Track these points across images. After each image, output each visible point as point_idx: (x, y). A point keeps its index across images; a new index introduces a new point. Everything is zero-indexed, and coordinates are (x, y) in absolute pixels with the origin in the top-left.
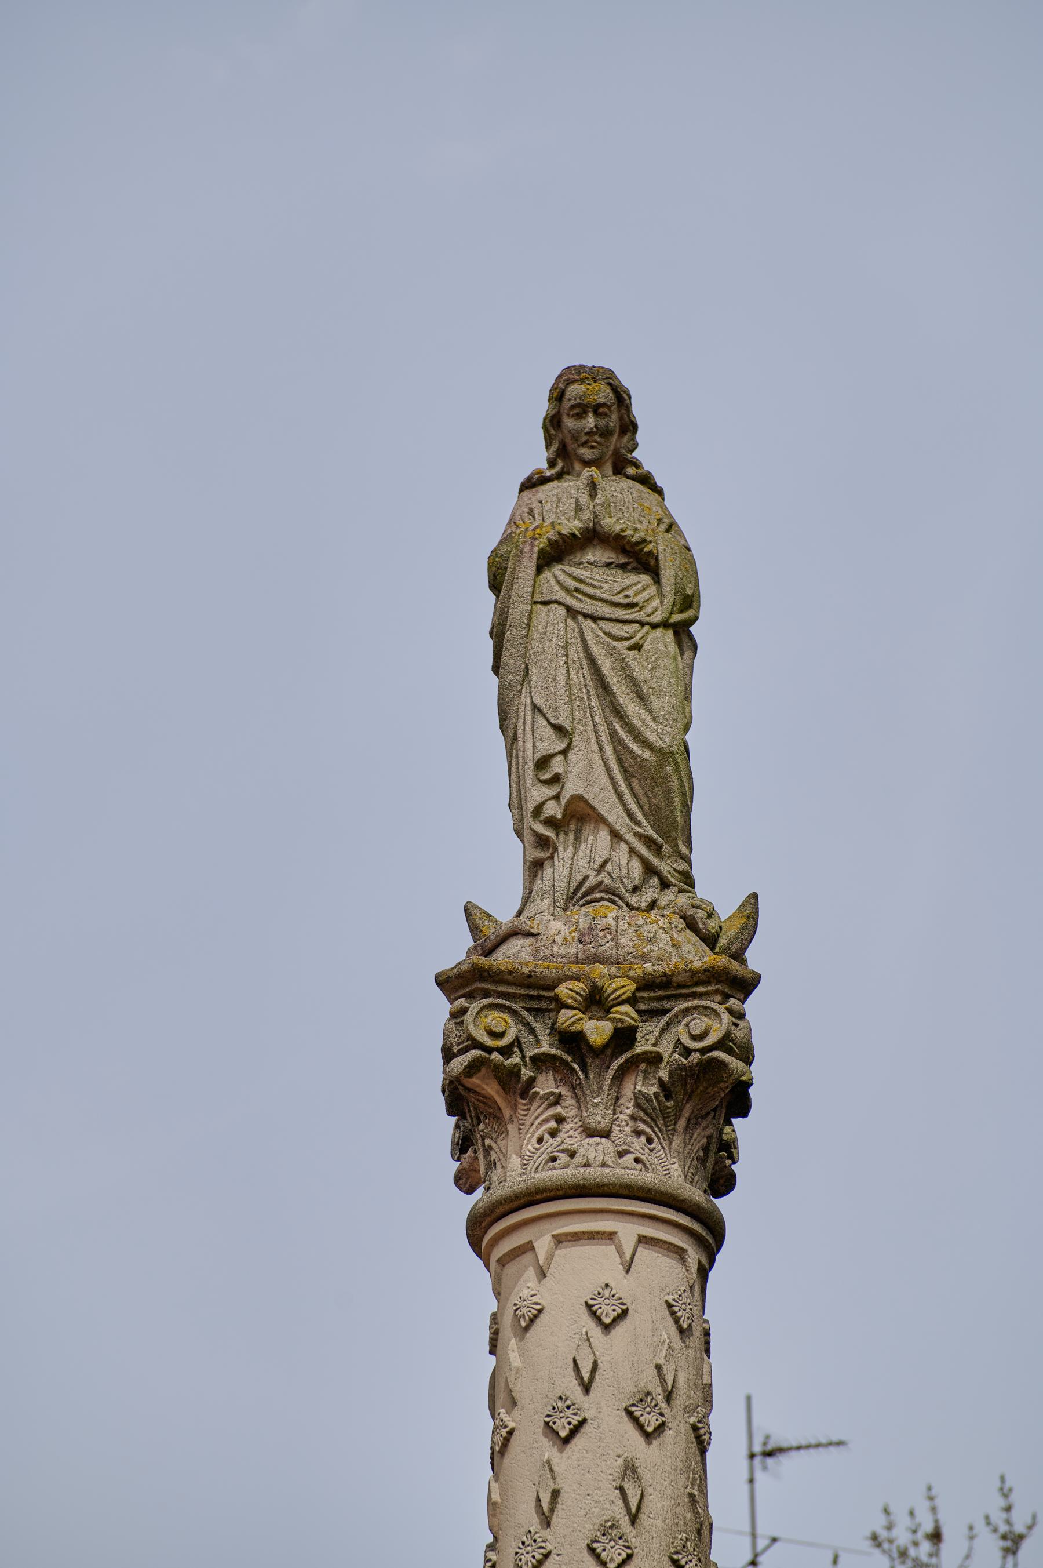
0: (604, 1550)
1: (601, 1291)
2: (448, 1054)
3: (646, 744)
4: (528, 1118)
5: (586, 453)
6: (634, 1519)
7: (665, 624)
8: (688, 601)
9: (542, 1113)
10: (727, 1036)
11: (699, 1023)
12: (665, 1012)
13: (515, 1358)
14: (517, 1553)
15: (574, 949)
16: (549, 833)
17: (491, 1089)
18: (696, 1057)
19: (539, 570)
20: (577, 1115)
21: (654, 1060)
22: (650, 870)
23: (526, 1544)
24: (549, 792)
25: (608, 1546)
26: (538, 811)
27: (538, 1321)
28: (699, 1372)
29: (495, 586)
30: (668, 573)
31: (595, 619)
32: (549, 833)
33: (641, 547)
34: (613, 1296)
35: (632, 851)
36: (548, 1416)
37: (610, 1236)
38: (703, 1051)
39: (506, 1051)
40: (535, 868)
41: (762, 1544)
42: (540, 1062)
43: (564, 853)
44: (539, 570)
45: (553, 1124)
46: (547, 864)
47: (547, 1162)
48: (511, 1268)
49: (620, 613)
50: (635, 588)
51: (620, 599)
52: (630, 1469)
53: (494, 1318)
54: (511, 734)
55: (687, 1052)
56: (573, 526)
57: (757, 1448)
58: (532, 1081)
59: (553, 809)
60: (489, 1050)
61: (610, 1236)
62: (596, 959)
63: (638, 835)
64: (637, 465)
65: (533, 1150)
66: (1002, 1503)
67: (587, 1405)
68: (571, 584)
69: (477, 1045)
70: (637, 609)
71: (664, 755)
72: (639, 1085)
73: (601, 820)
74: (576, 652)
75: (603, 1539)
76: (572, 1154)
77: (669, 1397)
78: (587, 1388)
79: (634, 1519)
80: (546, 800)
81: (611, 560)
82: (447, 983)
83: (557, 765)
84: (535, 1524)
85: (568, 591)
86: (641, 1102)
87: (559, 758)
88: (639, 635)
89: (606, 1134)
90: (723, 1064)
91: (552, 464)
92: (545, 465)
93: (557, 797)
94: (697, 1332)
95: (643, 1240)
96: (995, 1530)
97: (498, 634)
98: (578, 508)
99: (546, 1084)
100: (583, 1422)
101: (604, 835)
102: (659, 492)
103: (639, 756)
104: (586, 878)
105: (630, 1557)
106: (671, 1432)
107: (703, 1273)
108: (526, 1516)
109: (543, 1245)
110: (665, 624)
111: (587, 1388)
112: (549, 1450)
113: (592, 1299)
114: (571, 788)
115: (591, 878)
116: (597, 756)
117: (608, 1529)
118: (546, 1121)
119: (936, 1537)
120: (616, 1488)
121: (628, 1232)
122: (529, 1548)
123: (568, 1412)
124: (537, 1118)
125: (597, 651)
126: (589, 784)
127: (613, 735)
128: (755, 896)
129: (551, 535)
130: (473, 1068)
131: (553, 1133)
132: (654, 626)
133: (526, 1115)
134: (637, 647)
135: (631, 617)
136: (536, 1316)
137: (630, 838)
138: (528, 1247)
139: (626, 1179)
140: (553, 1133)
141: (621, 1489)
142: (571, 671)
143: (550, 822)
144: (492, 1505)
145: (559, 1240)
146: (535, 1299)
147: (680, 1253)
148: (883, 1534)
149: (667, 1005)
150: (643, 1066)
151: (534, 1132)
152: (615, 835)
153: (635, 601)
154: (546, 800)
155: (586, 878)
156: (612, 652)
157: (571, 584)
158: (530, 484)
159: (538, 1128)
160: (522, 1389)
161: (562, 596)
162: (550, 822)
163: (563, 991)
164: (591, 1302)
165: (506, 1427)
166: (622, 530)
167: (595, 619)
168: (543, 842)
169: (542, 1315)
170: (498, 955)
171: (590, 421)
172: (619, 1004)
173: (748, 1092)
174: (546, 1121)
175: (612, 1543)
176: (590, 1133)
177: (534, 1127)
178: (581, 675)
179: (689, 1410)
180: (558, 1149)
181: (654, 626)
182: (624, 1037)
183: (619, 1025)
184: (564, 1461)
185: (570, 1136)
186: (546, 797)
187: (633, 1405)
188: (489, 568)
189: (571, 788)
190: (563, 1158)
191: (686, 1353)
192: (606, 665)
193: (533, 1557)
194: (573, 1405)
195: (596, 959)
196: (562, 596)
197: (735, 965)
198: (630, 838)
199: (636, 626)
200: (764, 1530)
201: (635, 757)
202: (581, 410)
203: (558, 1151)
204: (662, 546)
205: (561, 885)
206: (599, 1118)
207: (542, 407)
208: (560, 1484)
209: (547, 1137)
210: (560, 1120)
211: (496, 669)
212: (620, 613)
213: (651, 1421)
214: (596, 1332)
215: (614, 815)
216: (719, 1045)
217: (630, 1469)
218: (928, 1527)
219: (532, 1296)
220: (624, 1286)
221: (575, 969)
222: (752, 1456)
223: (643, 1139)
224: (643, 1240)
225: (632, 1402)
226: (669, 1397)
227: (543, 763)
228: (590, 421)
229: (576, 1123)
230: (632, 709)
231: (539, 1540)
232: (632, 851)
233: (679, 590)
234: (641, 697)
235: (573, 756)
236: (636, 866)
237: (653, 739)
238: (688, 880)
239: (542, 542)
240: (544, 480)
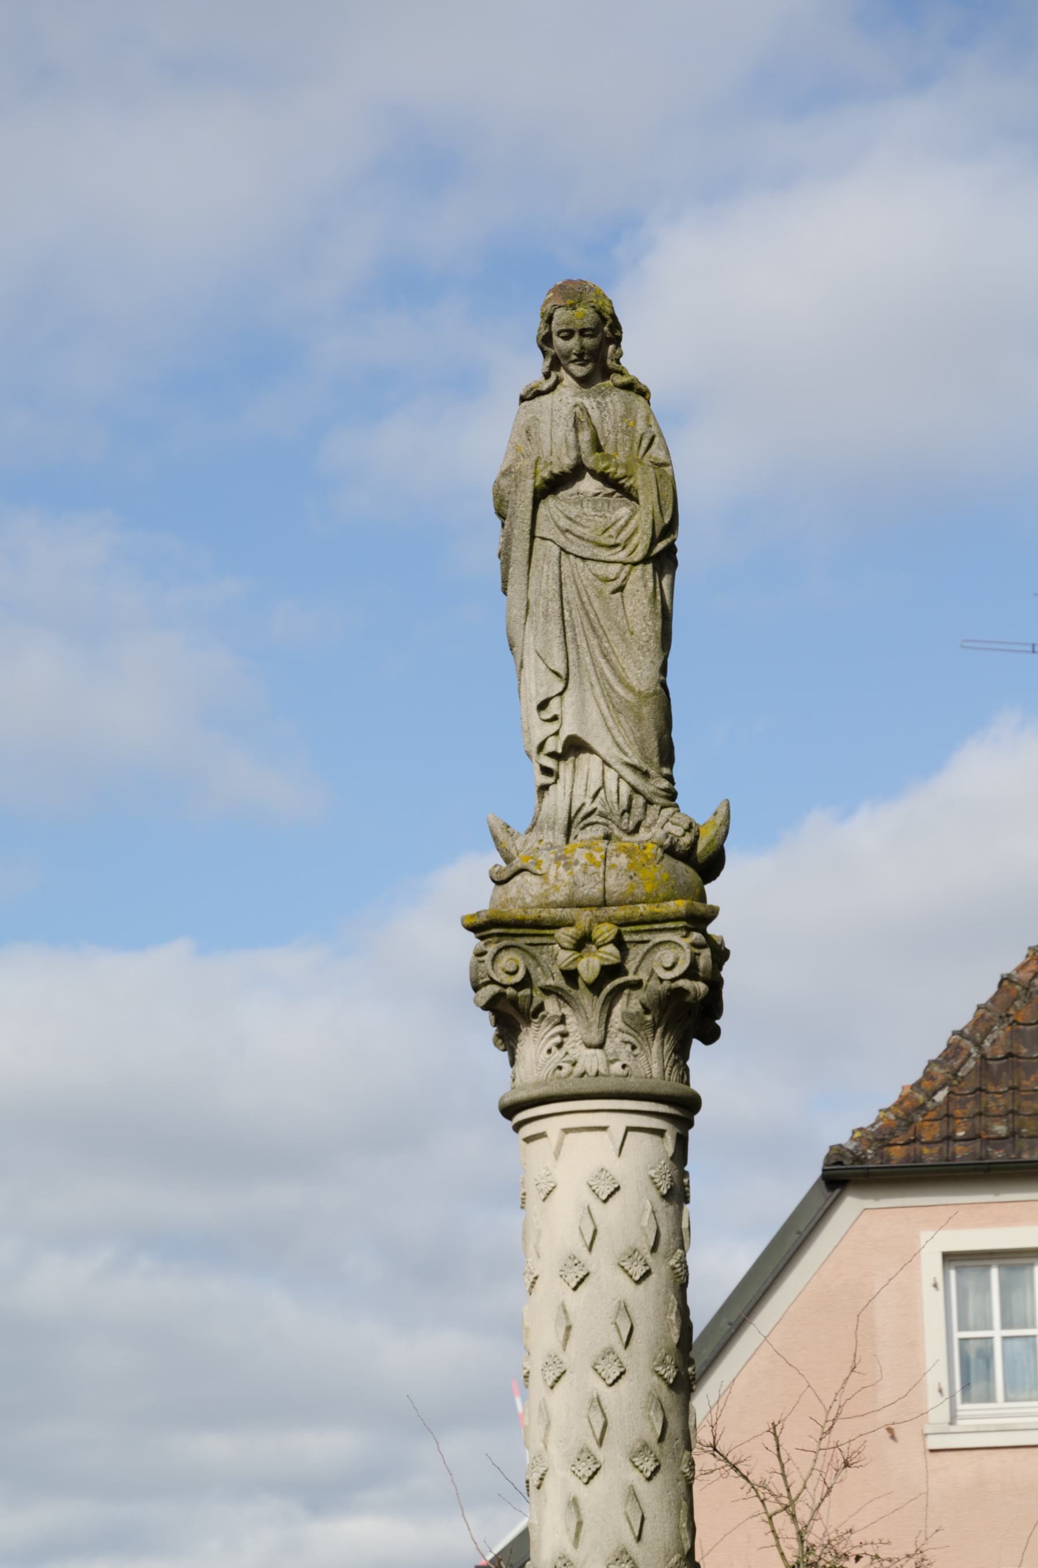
0: (603, 1370)
1: (598, 1174)
2: (476, 988)
3: (629, 688)
4: (539, 1032)
7: (645, 561)
9: (549, 1030)
11: (667, 956)
12: (647, 942)
14: (542, 1370)
16: (550, 763)
18: (666, 984)
20: (577, 1031)
21: (637, 985)
23: (549, 1364)
24: (553, 727)
25: (606, 1368)
26: (541, 747)
27: (551, 1194)
29: (502, 516)
32: (550, 763)
33: (623, 481)
34: (608, 1177)
36: (561, 1271)
37: (604, 1129)
38: (673, 980)
45: (558, 1039)
46: (551, 788)
47: (555, 1070)
50: (615, 528)
51: (604, 540)
52: (624, 1308)
54: (519, 662)
56: (567, 462)
59: (551, 746)
60: (505, 986)
61: (604, 1129)
63: (628, 765)
65: (544, 1060)
70: (619, 549)
72: (628, 1004)
73: (592, 751)
75: (603, 1362)
76: (574, 1064)
80: (548, 737)
81: (598, 491)
83: (553, 708)
87: (556, 700)
88: (623, 576)
89: (601, 1046)
92: (540, 377)
93: (557, 733)
96: (840, 1526)
99: (552, 1006)
100: (588, 1275)
102: (644, 393)
103: (622, 697)
104: (583, 805)
105: (622, 1373)
106: (640, 1327)
107: (682, 1143)
113: (593, 1181)
115: (587, 805)
116: (588, 694)
117: (610, 1351)
118: (553, 1036)
120: (612, 1324)
121: (618, 1123)
122: (551, 1368)
123: (576, 1268)
124: (546, 1034)
129: (546, 474)
131: (560, 1046)
132: (635, 564)
133: (538, 1031)
135: (612, 558)
136: (551, 1191)
137: (618, 766)
140: (560, 1046)
141: (616, 1324)
142: (565, 611)
143: (553, 755)
146: (550, 1178)
147: (661, 1133)
149: (646, 937)
150: (626, 991)
151: (544, 1045)
153: (618, 541)
154: (548, 737)
155: (583, 805)
157: (564, 523)
159: (547, 1041)
162: (553, 755)
164: (591, 1183)
165: (532, 1274)
166: (606, 468)
168: (546, 771)
169: (555, 1190)
170: (590, 503)
172: (605, 945)
173: (720, 975)
174: (553, 1036)
175: (609, 1365)
177: (544, 1040)
180: (563, 1060)
181: (635, 564)
183: (606, 963)
185: (575, 1047)
186: (547, 735)
187: (624, 1261)
188: (495, 498)
190: (567, 1067)
193: (554, 1374)
194: (579, 1262)
197: (698, 905)
198: (618, 766)
199: (618, 566)
201: (618, 695)
203: (564, 1062)
204: (642, 481)
208: (572, 1321)
209: (554, 1049)
210: (564, 1035)
211: (505, 591)
212: (604, 554)
214: (597, 1207)
217: (624, 1308)
219: (548, 1175)
223: (629, 1047)
224: (629, 1129)
225: (623, 1259)
229: (577, 1037)
231: (558, 1362)
232: (620, 777)
236: (625, 789)
237: (635, 683)
240: (538, 393)
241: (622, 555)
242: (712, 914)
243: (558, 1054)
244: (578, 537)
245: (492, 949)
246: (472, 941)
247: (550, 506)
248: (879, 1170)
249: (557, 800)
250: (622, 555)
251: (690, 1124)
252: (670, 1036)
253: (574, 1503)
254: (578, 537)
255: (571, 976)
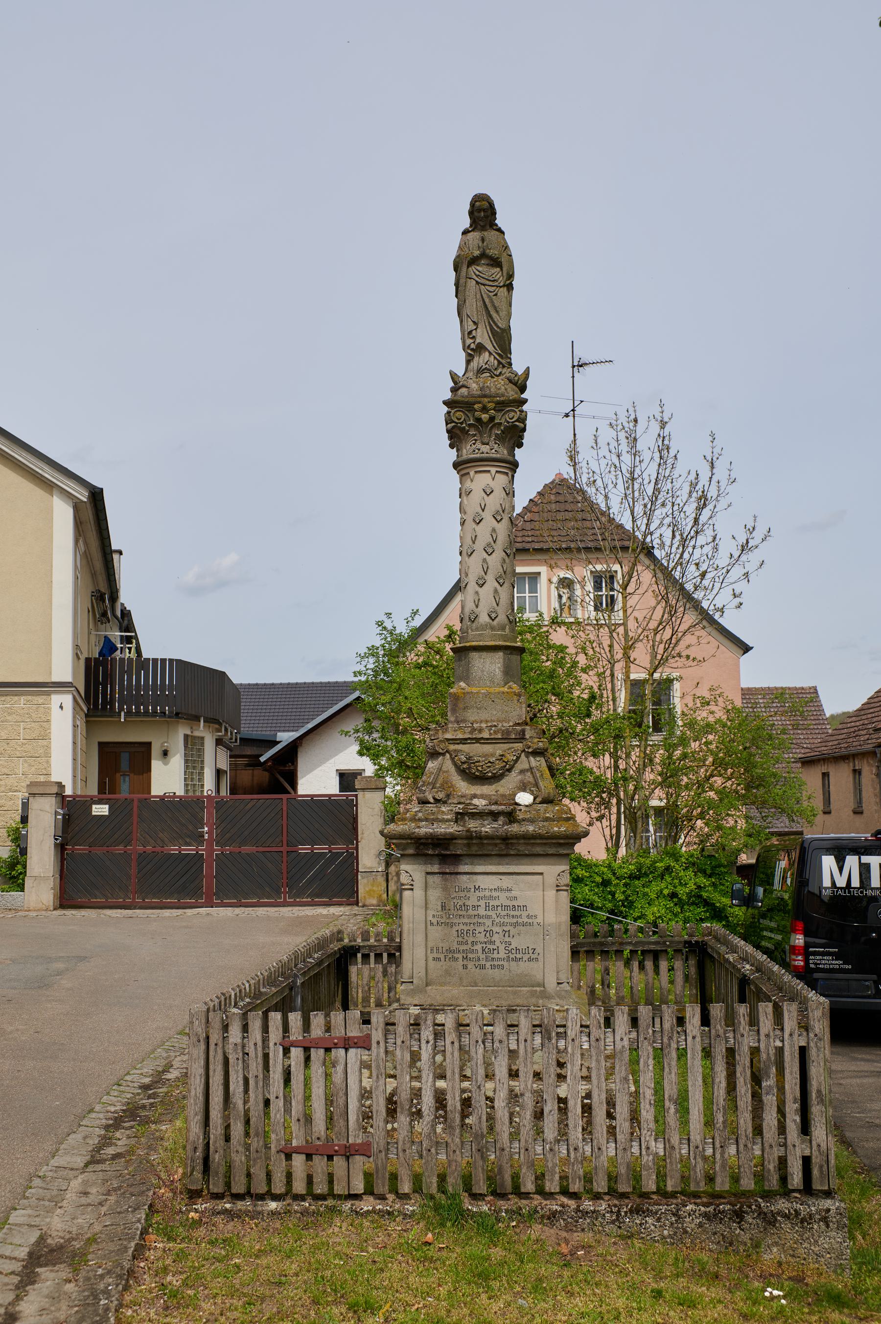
2: (447, 424)
3: (498, 327)
5: (482, 223)
6: (495, 542)
7: (504, 286)
8: (511, 276)
10: (519, 418)
13: (465, 502)
15: (479, 393)
17: (458, 432)
19: (468, 267)
22: (499, 363)
24: (472, 341)
26: (469, 346)
28: (511, 503)
30: (505, 269)
31: (484, 285)
35: (495, 358)
37: (489, 471)
39: (461, 423)
40: (468, 362)
41: (576, 403)
42: (470, 425)
43: (476, 359)
44: (468, 267)
48: (464, 478)
49: (491, 283)
52: (494, 530)
53: (460, 489)
55: (508, 422)
56: (477, 253)
57: (576, 363)
58: (468, 431)
59: (473, 346)
61: (489, 471)
62: (485, 396)
64: (496, 225)
66: (660, 410)
67: (484, 515)
68: (477, 273)
69: (454, 422)
71: (503, 330)
73: (486, 349)
74: (479, 296)
77: (503, 511)
78: (483, 511)
79: (495, 542)
82: (445, 403)
83: (474, 333)
84: (471, 543)
85: (477, 276)
86: (496, 435)
89: (488, 444)
90: (517, 426)
91: (471, 226)
94: (511, 493)
95: (497, 472)
97: (457, 285)
98: (479, 247)
101: (487, 354)
102: (503, 233)
107: (513, 477)
108: (468, 541)
109: (472, 473)
110: (504, 286)
111: (483, 511)
112: (474, 526)
114: (478, 341)
117: (489, 545)
119: (636, 421)
121: (493, 470)
125: (485, 296)
126: (483, 338)
127: (489, 323)
128: (528, 368)
130: (453, 427)
134: (496, 295)
138: (468, 473)
139: (503, 395)
143: (472, 350)
144: (461, 537)
145: (476, 472)
147: (507, 474)
148: (614, 423)
152: (490, 354)
156: (489, 296)
157: (477, 273)
158: (465, 232)
160: (467, 509)
161: (474, 277)
162: (472, 350)
163: (476, 406)
167: (484, 285)
168: (469, 355)
171: (482, 214)
176: (483, 444)
178: (480, 303)
179: (509, 513)
182: (492, 419)
184: (478, 528)
189: (478, 341)
191: (508, 499)
192: (487, 300)
195: (485, 396)
196: (474, 277)
200: (571, 418)
202: (479, 210)
204: (504, 260)
205: (475, 368)
206: (486, 441)
207: (468, 207)
210: (476, 440)
211: (456, 296)
212: (491, 283)
213: (499, 518)
214: (485, 496)
215: (490, 347)
216: (517, 421)
217: (494, 530)
218: (632, 417)
220: (492, 484)
221: (479, 399)
222: (574, 367)
226: (503, 511)
227: (470, 333)
228: (482, 214)
230: (494, 315)
232: (495, 358)
233: (508, 274)
234: (497, 312)
235: (478, 330)
236: (496, 362)
238: (510, 364)
239: (468, 259)
241: (496, 284)
242: (525, 401)
243: (474, 446)
244: (387, 881)
245: (453, 411)
246: (445, 409)
247: (473, 268)
248: (310, 726)
249: (474, 364)
250: (496, 284)
251: (515, 472)
252: (250, 990)
253: (477, 593)
254: (387, 881)
255: (479, 420)
